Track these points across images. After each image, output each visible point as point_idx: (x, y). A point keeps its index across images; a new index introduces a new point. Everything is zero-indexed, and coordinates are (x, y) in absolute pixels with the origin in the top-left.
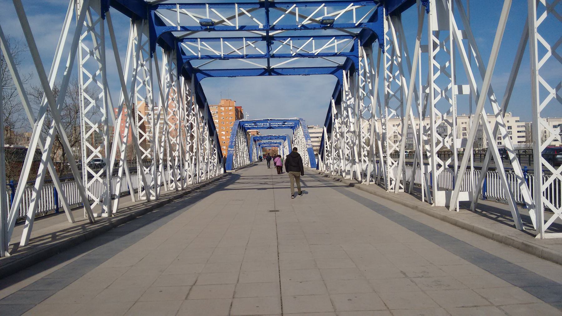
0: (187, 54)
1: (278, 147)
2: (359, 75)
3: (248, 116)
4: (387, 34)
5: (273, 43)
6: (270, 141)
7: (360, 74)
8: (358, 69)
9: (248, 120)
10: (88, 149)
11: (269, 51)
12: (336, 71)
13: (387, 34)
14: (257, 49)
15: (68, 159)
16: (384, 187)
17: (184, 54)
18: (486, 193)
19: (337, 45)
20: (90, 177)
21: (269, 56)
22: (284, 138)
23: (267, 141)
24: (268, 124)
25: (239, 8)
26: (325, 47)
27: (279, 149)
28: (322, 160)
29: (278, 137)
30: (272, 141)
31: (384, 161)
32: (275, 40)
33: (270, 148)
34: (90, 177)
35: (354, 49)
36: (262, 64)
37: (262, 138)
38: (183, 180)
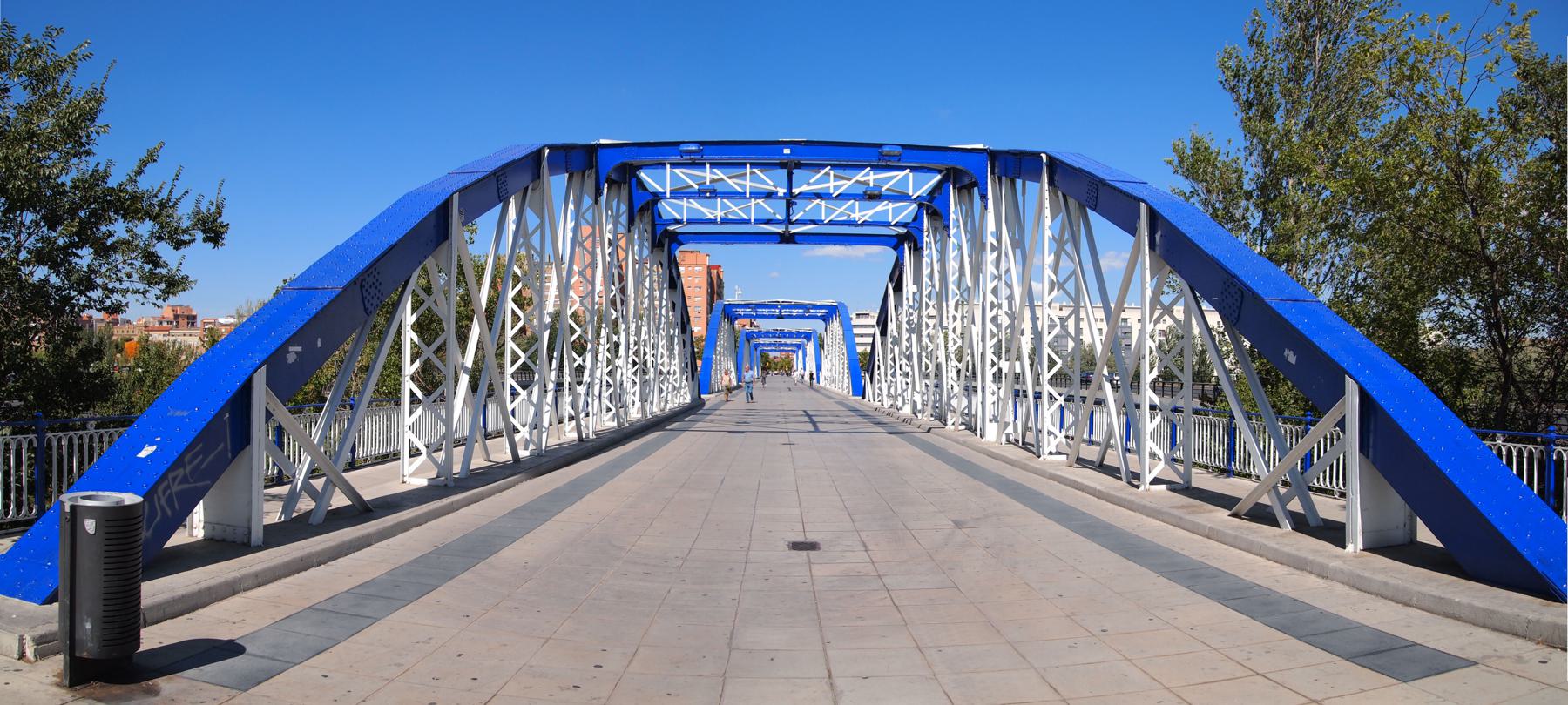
0: (665, 217)
1: (794, 352)
2: (949, 236)
3: (740, 292)
4: (954, 212)
5: (796, 204)
6: (778, 340)
7: (951, 235)
8: (922, 248)
9: (740, 303)
10: (513, 352)
11: (788, 215)
12: (897, 242)
13: (954, 212)
14: (772, 211)
15: (1117, 365)
16: (1034, 450)
17: (660, 216)
18: (1233, 463)
19: (893, 208)
20: (514, 394)
21: (789, 221)
22: (808, 336)
23: (773, 340)
24: (777, 311)
25: (751, 168)
26: (871, 212)
27: (795, 357)
28: (871, 382)
29: (798, 334)
30: (783, 340)
31: (1035, 393)
32: (841, 403)
33: (778, 354)
34: (514, 394)
35: (917, 218)
36: (780, 229)
37: (760, 334)
38: (536, 430)
